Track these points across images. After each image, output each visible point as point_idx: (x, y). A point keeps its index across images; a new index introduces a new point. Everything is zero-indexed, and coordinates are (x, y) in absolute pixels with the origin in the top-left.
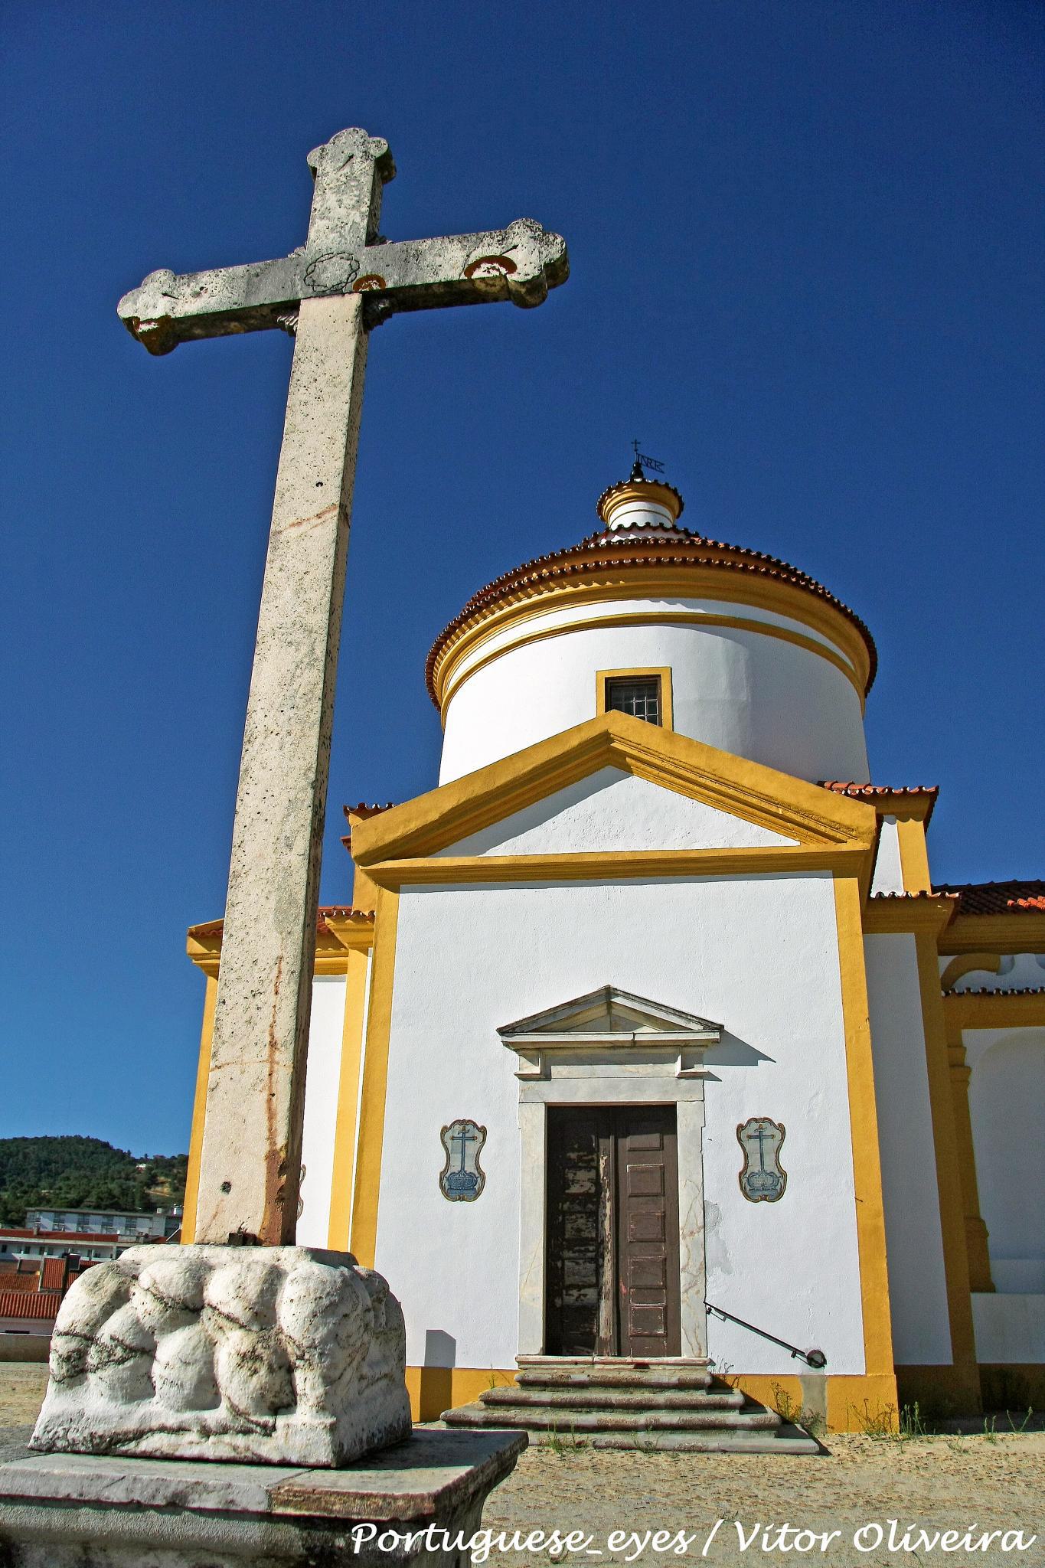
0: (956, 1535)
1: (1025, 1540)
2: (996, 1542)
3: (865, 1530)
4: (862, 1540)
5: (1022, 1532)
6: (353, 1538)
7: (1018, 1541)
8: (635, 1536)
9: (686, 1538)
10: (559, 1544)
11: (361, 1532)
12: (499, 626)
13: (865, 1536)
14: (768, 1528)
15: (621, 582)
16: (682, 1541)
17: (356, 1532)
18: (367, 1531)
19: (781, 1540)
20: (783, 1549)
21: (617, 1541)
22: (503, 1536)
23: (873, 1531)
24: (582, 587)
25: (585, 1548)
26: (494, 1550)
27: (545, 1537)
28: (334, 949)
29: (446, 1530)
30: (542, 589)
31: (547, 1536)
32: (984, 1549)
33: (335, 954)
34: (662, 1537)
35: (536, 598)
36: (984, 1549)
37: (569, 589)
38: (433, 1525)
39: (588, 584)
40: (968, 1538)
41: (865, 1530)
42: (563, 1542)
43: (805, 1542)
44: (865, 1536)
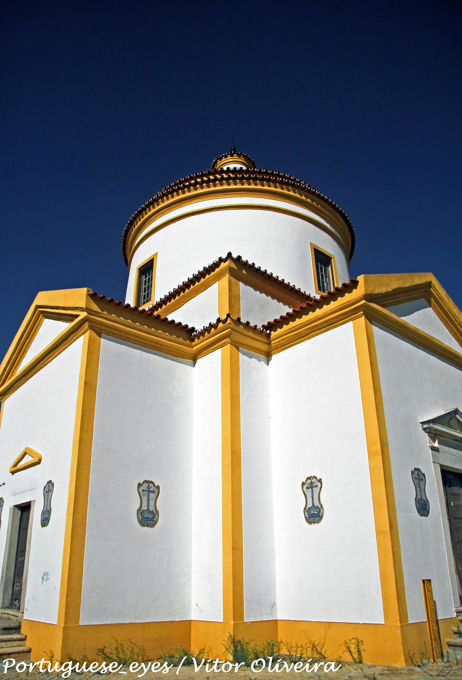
0: (97, 664)
1: (336, 667)
2: (321, 668)
3: (257, 661)
4: (255, 667)
5: (71, 662)
6: (4, 666)
7: (332, 667)
8: (143, 665)
9: (168, 666)
10: (105, 669)
11: (7, 662)
12: (249, 193)
13: (257, 664)
14: (209, 661)
15: (319, 206)
16: (166, 667)
17: (5, 662)
18: (10, 662)
19: (215, 667)
20: (216, 671)
21: (94, 667)
22: (78, 665)
23: (260, 662)
24: (303, 198)
25: (119, 671)
26: (74, 671)
27: (160, 666)
28: (183, 340)
29: (49, 662)
30: (296, 191)
31: (100, 665)
32: (315, 671)
33: (182, 343)
34: (156, 665)
35: (279, 190)
36: (315, 671)
37: (297, 195)
38: (43, 659)
39: (313, 201)
40: (307, 665)
41: (257, 661)
42: (107, 668)
43: (227, 667)
44: (257, 664)
